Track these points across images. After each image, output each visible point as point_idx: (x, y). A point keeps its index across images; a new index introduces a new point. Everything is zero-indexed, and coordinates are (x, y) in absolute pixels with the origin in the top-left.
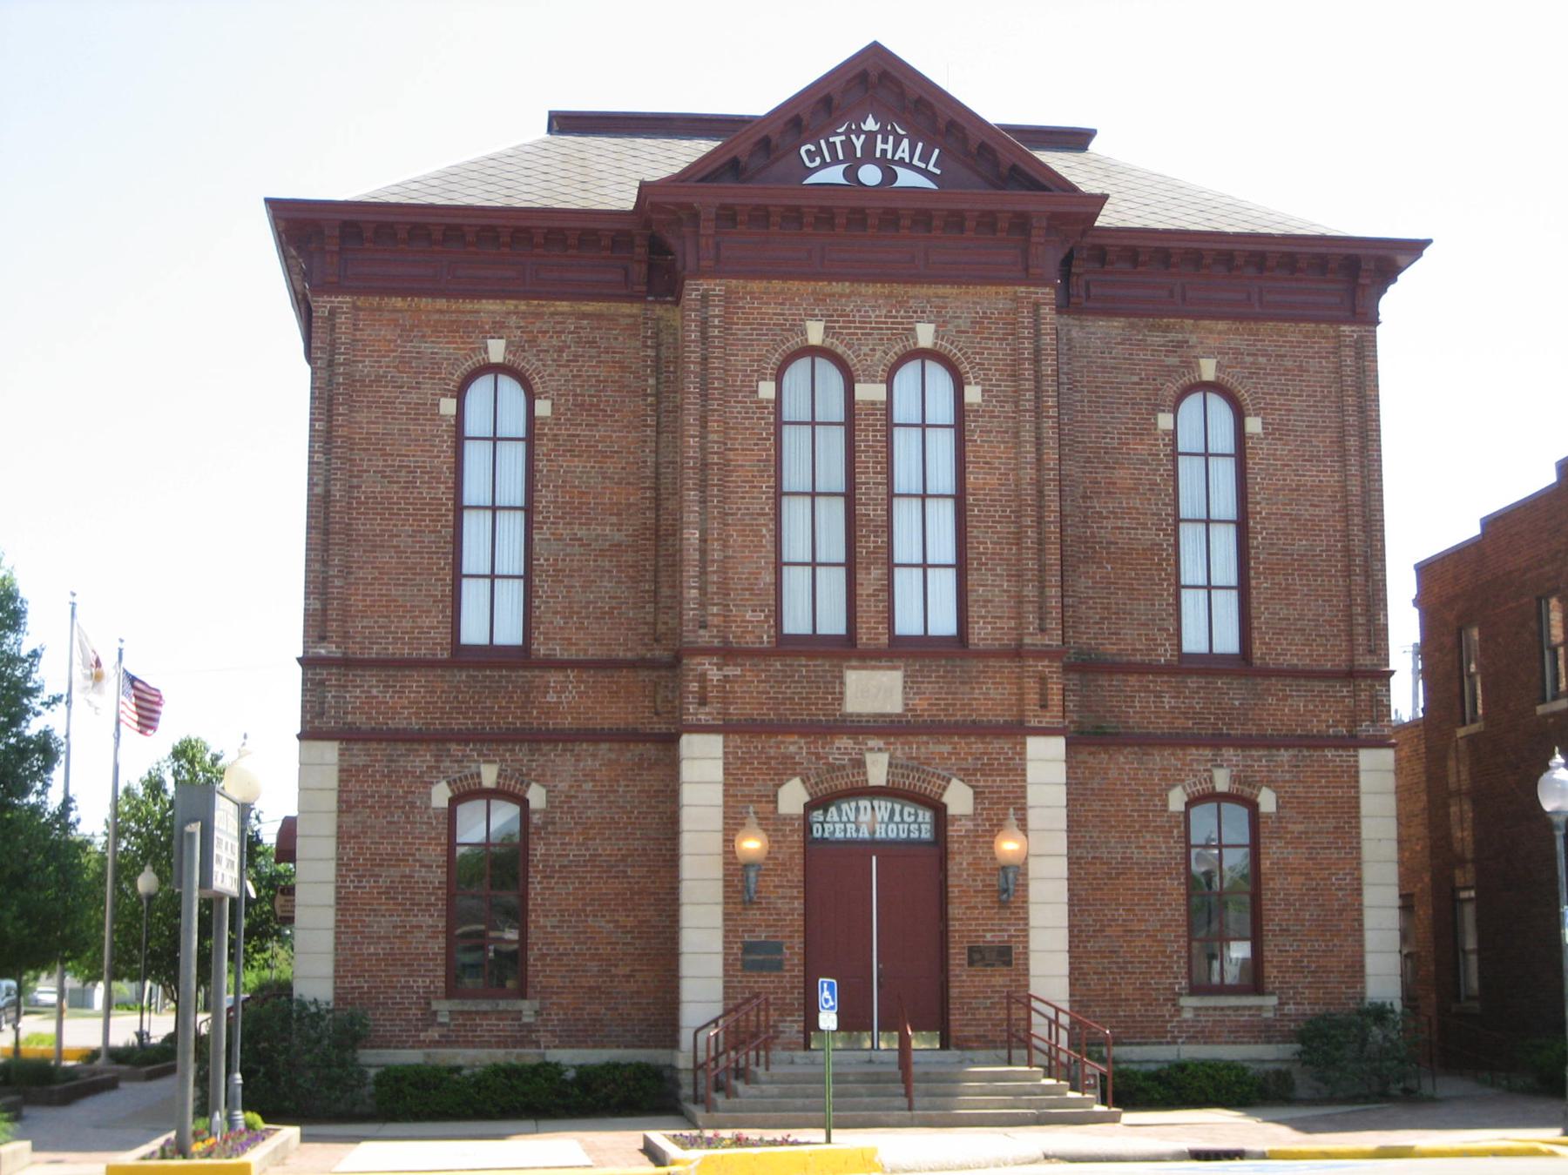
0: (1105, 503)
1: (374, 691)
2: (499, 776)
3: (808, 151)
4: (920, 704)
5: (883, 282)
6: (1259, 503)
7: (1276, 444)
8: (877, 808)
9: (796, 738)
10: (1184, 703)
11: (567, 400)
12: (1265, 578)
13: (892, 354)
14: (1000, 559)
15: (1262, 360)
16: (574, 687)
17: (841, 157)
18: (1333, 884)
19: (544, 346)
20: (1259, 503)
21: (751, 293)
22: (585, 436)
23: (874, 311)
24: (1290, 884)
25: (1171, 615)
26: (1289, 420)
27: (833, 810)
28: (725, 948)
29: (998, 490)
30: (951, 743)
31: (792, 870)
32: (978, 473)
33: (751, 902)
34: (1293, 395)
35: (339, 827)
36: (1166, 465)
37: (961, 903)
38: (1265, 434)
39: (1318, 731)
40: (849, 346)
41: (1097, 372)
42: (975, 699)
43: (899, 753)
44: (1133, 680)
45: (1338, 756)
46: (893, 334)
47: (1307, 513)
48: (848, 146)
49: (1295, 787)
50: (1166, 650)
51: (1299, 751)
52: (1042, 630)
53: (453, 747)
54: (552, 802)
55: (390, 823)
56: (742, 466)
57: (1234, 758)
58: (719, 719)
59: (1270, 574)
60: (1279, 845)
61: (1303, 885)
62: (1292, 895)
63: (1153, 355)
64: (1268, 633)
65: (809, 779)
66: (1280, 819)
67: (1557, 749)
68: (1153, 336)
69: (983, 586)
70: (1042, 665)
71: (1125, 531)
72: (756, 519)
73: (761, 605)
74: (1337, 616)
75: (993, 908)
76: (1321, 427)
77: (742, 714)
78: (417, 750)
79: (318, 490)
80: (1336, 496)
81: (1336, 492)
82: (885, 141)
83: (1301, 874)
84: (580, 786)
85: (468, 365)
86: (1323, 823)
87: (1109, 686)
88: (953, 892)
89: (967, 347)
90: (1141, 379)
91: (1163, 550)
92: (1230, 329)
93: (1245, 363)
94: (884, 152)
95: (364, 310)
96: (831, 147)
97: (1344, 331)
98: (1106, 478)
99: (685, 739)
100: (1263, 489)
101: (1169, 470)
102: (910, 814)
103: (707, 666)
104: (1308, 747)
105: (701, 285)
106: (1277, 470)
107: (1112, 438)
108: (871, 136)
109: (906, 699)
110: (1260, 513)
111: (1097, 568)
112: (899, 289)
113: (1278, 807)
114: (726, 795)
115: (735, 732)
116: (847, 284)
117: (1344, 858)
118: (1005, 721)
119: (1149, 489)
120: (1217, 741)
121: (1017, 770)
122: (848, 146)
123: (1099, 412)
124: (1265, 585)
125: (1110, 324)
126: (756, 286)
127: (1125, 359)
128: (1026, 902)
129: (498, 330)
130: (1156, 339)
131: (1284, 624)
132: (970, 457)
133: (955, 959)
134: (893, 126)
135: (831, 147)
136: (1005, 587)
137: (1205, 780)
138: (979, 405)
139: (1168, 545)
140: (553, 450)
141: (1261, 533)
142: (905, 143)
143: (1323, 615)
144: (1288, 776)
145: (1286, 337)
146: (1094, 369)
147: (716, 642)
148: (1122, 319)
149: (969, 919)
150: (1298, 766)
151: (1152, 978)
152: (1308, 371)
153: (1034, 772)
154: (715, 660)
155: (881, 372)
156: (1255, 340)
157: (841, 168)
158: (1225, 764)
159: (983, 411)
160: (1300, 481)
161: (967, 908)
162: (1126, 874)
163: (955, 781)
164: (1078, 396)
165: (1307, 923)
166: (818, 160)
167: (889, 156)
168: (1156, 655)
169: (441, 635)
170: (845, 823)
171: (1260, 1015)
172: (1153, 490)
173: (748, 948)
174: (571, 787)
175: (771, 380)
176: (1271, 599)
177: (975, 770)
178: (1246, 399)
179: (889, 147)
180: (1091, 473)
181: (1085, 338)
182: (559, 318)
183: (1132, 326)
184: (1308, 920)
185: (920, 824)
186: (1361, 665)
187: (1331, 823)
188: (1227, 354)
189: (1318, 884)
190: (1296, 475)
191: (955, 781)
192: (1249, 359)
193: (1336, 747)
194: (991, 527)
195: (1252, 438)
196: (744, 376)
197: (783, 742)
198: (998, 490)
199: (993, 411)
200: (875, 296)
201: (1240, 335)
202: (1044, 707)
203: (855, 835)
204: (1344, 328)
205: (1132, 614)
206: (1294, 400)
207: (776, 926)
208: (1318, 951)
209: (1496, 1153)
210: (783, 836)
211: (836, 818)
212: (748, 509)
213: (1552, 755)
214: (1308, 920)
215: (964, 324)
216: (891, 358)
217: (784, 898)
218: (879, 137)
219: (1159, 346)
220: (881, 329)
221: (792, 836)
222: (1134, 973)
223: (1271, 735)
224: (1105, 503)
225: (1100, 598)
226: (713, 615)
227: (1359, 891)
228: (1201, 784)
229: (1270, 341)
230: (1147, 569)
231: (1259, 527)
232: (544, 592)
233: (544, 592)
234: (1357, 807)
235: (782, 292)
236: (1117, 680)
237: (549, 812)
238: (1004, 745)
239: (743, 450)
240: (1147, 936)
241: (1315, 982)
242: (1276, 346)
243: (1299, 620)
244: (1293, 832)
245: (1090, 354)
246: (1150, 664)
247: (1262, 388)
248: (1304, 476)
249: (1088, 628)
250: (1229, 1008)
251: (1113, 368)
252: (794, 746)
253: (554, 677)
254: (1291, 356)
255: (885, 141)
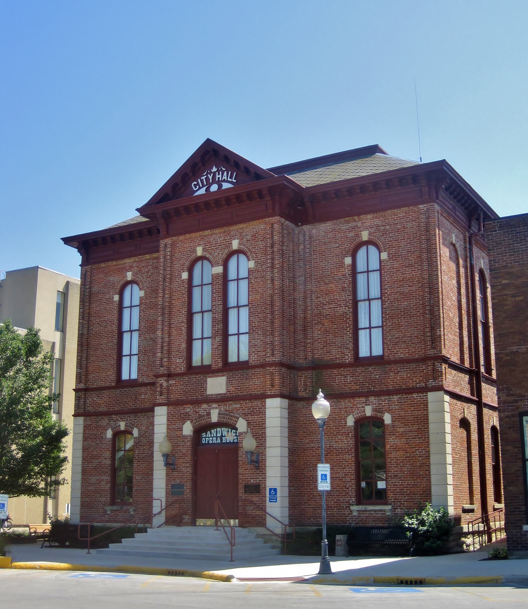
0: (325, 298)
1: (95, 399)
2: (126, 426)
3: (195, 184)
4: (232, 389)
5: (226, 226)
6: (386, 289)
7: (394, 262)
8: (230, 432)
9: (189, 406)
10: (355, 379)
11: (149, 290)
12: (389, 321)
13: (224, 254)
14: (260, 328)
15: (388, 227)
16: (149, 392)
17: (205, 184)
18: (417, 454)
19: (143, 271)
20: (386, 289)
21: (181, 241)
22: (154, 301)
23: (219, 239)
24: (398, 455)
25: (350, 342)
26: (399, 251)
27: (209, 432)
28: (166, 486)
29: (260, 300)
30: (240, 404)
31: (187, 456)
32: (253, 295)
33: (174, 469)
34: (400, 240)
35: (83, 446)
36: (349, 279)
37: (243, 467)
38: (389, 258)
39: (412, 386)
40: (210, 254)
41: (322, 245)
42: (251, 385)
43: (222, 409)
44: (335, 371)
45: (419, 396)
46: (225, 246)
47: (406, 290)
48: (207, 179)
49: (400, 412)
50: (349, 357)
51: (402, 395)
52: (273, 355)
53: (114, 416)
54: (140, 434)
55: (96, 444)
56: (177, 305)
57: (374, 401)
58: (166, 400)
59: (391, 319)
60: (393, 438)
61: (404, 455)
62: (400, 460)
63: (344, 234)
64: (390, 345)
65: (193, 421)
66: (393, 426)
67: (320, 390)
68: (344, 226)
69: (254, 339)
70: (271, 369)
71: (332, 309)
72: (180, 324)
73: (181, 356)
74: (420, 334)
75: (253, 469)
76: (413, 251)
77: (175, 398)
78: (104, 418)
79: (80, 332)
80: (420, 280)
81: (420, 279)
82: (219, 174)
83: (403, 450)
84: (149, 428)
85: (122, 282)
86: (413, 427)
87: (326, 374)
88: (240, 463)
89: (250, 246)
90: (339, 245)
91: (348, 315)
92: (373, 217)
93: (381, 230)
94: (219, 178)
95: (95, 269)
96: (202, 181)
97: (421, 208)
98: (325, 288)
99: (156, 408)
100: (388, 282)
101: (350, 281)
102: (234, 433)
103: (163, 381)
104: (406, 394)
105: (164, 241)
106: (394, 273)
107: (328, 271)
108: (214, 173)
109: (227, 387)
110: (387, 293)
111: (322, 326)
112: (226, 229)
113: (393, 421)
114: (168, 429)
115: (171, 405)
116: (209, 231)
117: (422, 443)
118: (261, 393)
119: (342, 290)
120: (367, 395)
121: (262, 412)
122: (207, 179)
123: (323, 262)
124: (389, 324)
125: (326, 225)
126: (181, 238)
127: (333, 238)
128: (265, 466)
129: (130, 268)
130: (344, 227)
131: (397, 340)
132: (185, 296)
133: (240, 490)
134: (221, 168)
135: (202, 181)
136: (262, 339)
137: (362, 411)
138: (254, 268)
139: (349, 312)
140: (145, 308)
141: (388, 302)
142: (225, 173)
143: (414, 334)
144: (397, 407)
145: (398, 215)
146: (321, 244)
147: (166, 372)
148: (329, 222)
149: (245, 474)
150: (401, 402)
151: (341, 498)
152: (407, 228)
153: (269, 413)
154: (165, 379)
155: (221, 262)
156: (385, 219)
157: (205, 188)
158: (370, 404)
159: (255, 270)
160: (404, 276)
161: (245, 469)
162: (331, 453)
163: (240, 419)
164: (315, 256)
165: (405, 472)
166: (198, 187)
167: (220, 180)
168: (345, 359)
169: (113, 377)
170: (212, 437)
171: (385, 514)
172: (343, 290)
173: (173, 486)
174: (146, 428)
175: (186, 271)
176: (392, 330)
177: (248, 414)
178: (380, 245)
179: (220, 176)
180: (320, 287)
181: (317, 232)
182: (148, 261)
183: (335, 224)
184: (406, 471)
185: (237, 436)
186: (429, 354)
187: (416, 427)
188: (374, 227)
189: (410, 455)
190: (402, 274)
191: (240, 419)
192: (382, 228)
193: (418, 393)
194: (257, 316)
195: (384, 261)
196: (178, 272)
197: (186, 408)
198: (260, 300)
199: (259, 270)
200: (220, 233)
201: (378, 218)
202: (273, 386)
203: (216, 442)
204: (420, 206)
205: (335, 343)
206: (402, 242)
207: (182, 478)
208: (410, 485)
209: (46, 569)
210: (185, 443)
211: (210, 436)
212: (178, 321)
213: (318, 393)
214: (406, 471)
215: (249, 237)
216: (225, 256)
217: (185, 467)
218: (217, 173)
219: (346, 230)
220: (221, 245)
221: (188, 443)
222: (334, 495)
223: (392, 389)
224: (325, 298)
225: (323, 338)
226: (165, 362)
227: (428, 457)
228: (360, 413)
229: (391, 218)
230: (341, 324)
231: (386, 299)
232: (141, 359)
233: (141, 359)
234: (427, 419)
235: (190, 238)
236: (329, 371)
237: (140, 438)
238: (258, 403)
239: (177, 299)
240: (339, 480)
241: (409, 499)
242: (394, 220)
243: (403, 337)
244: (399, 432)
245: (320, 238)
246: (342, 364)
247: (388, 239)
248: (406, 274)
249: (319, 351)
250: (372, 510)
251: (328, 242)
252: (189, 409)
253: (143, 389)
254: (400, 223)
255: (219, 174)
